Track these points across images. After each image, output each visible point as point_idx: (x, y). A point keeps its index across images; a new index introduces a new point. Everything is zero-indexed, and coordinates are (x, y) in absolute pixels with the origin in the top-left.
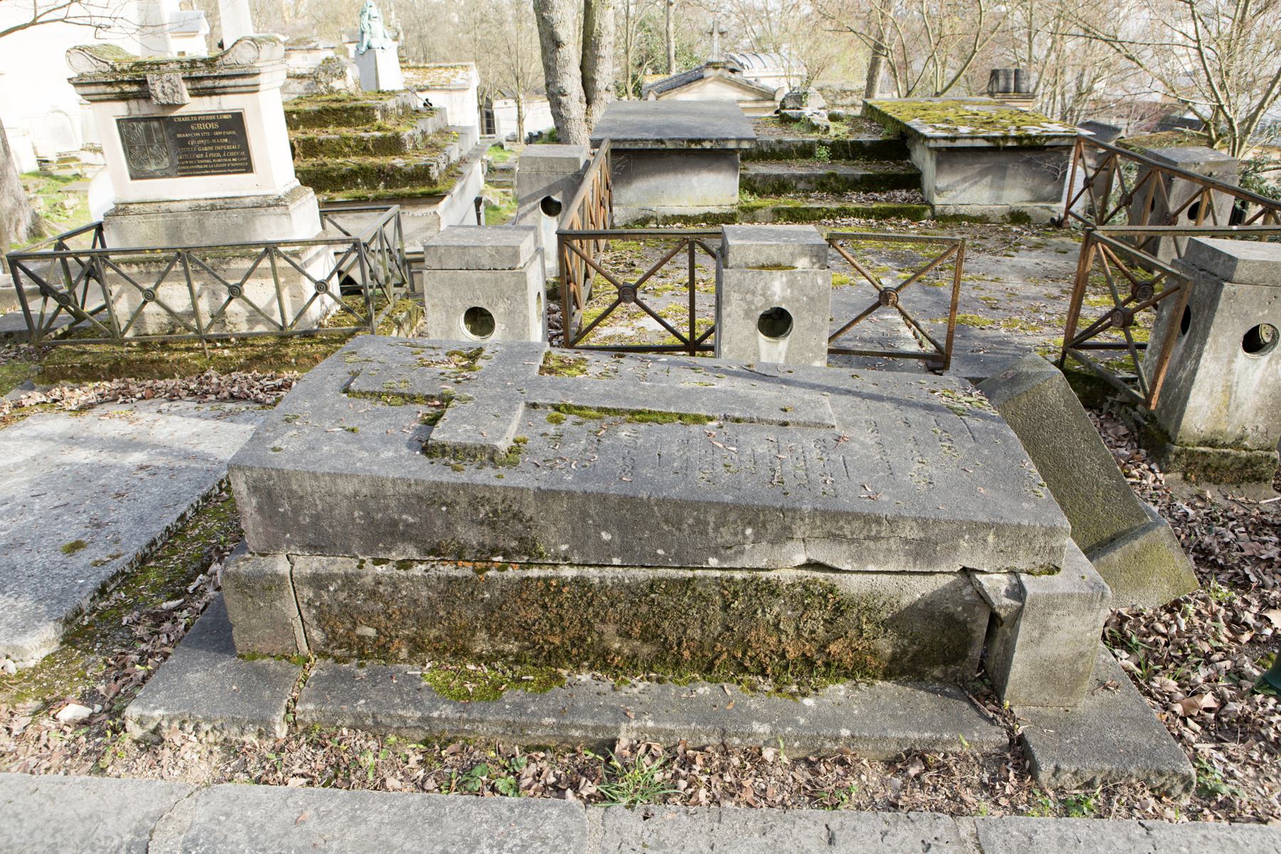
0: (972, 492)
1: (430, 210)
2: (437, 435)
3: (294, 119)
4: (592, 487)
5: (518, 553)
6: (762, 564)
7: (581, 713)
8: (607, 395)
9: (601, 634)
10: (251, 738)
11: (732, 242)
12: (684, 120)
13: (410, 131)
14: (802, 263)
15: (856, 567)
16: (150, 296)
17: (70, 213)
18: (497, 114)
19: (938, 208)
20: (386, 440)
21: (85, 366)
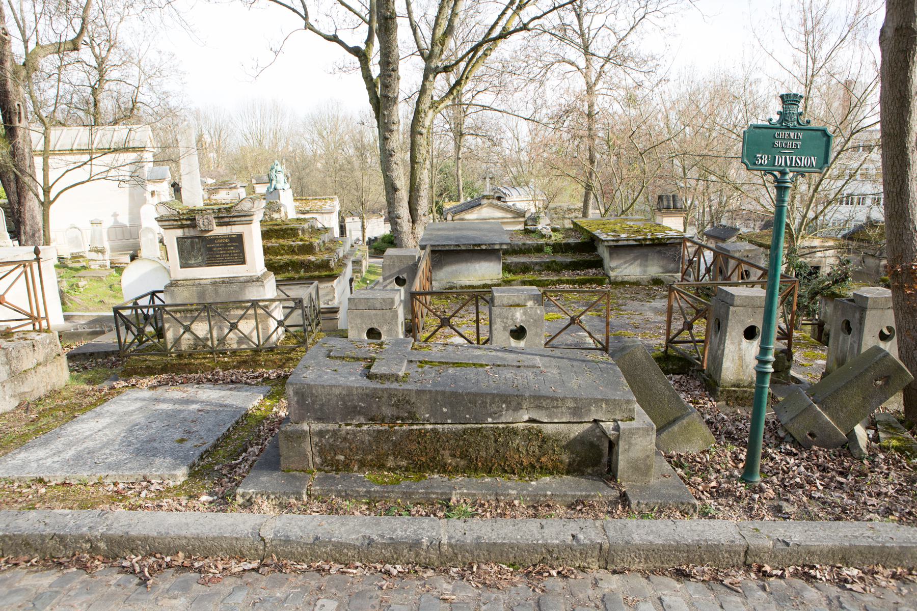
0: (597, 389)
1: (329, 284)
2: (373, 370)
3: (266, 235)
4: (439, 389)
5: (408, 419)
6: (510, 420)
7: (435, 488)
8: (442, 357)
9: (443, 455)
10: (293, 501)
11: (495, 294)
12: (470, 233)
13: (318, 241)
14: (530, 303)
15: (549, 420)
16: (187, 329)
17: (82, 290)
18: (348, 227)
19: (612, 278)
20: (350, 374)
21: (148, 367)
